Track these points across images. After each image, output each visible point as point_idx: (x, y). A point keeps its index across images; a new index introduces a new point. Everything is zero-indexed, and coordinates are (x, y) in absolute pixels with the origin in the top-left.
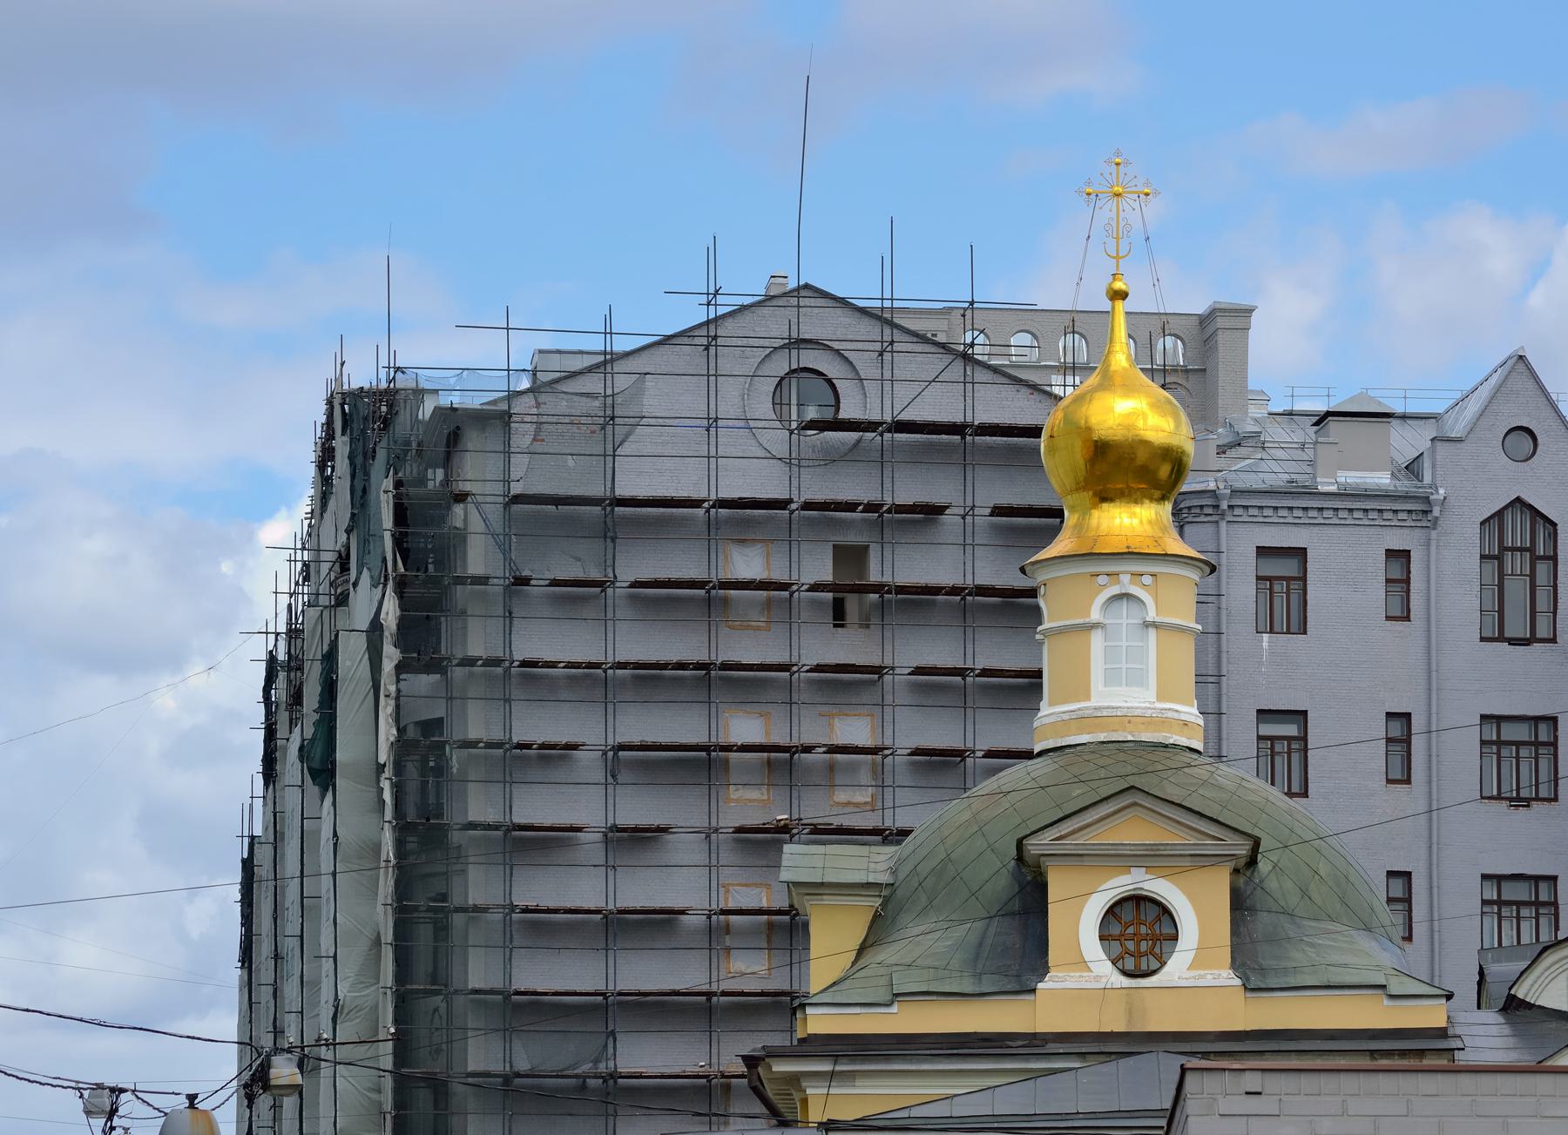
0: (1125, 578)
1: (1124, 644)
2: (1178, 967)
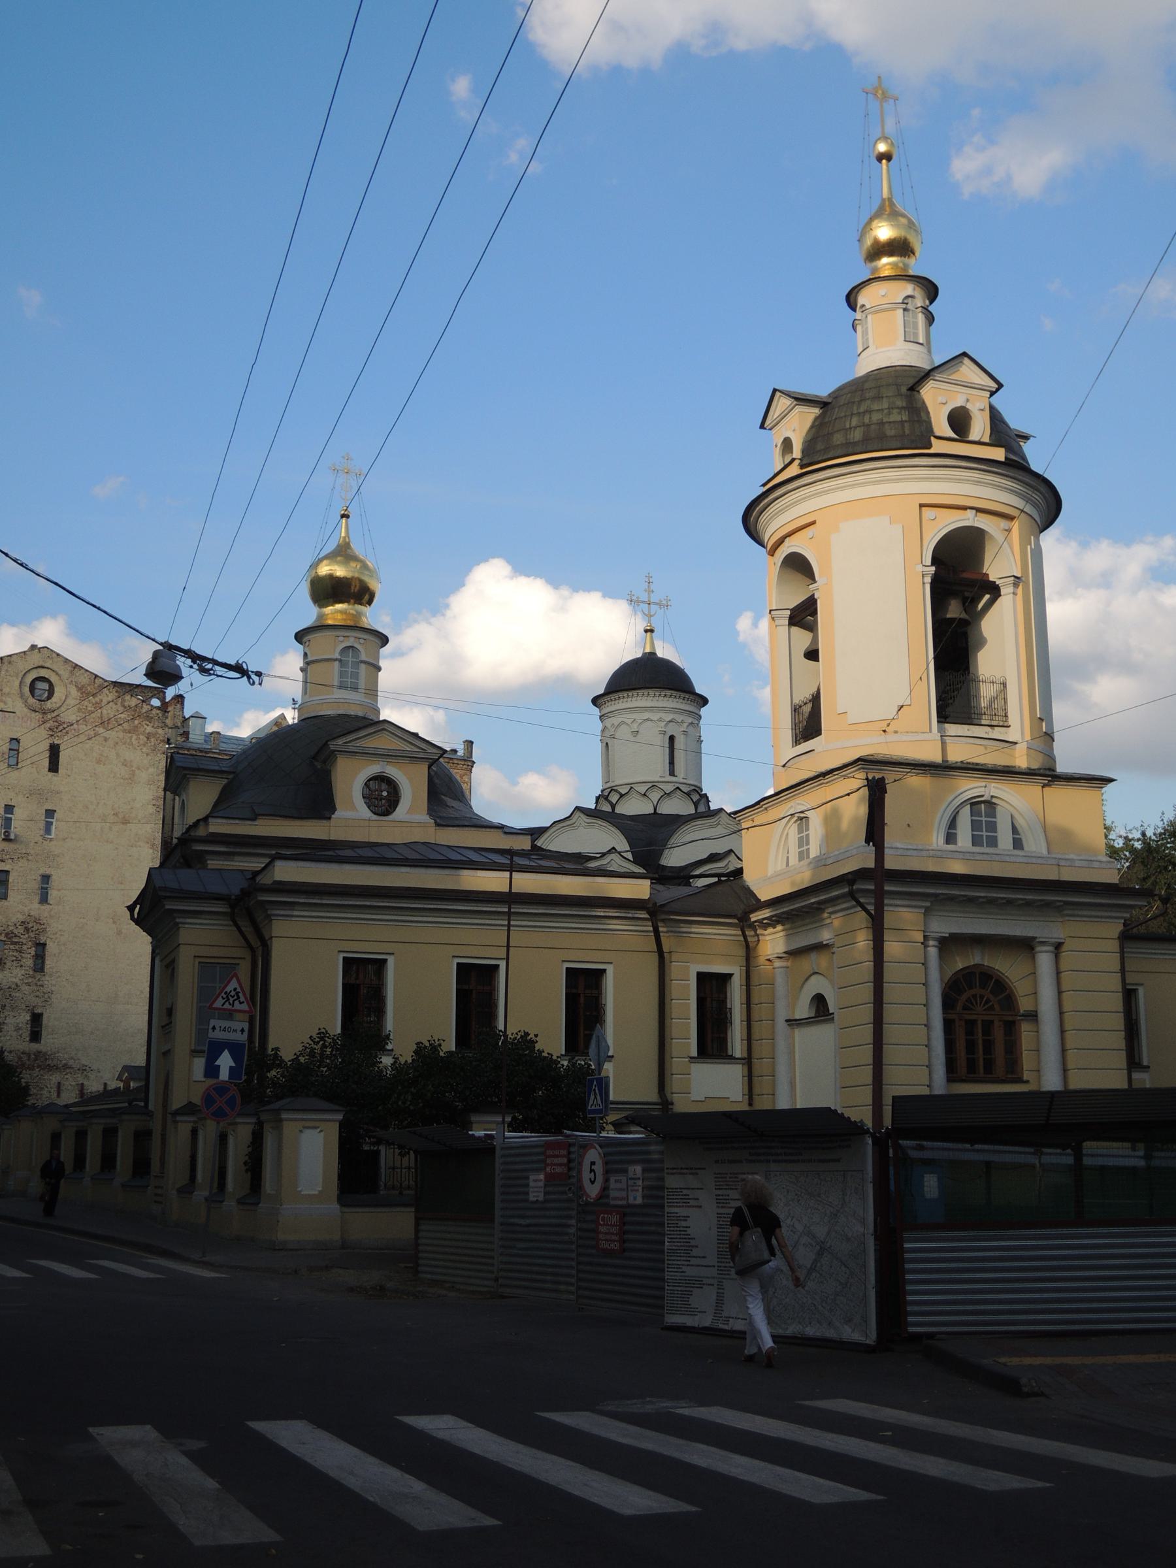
0: (352, 639)
1: (350, 670)
2: (401, 812)
